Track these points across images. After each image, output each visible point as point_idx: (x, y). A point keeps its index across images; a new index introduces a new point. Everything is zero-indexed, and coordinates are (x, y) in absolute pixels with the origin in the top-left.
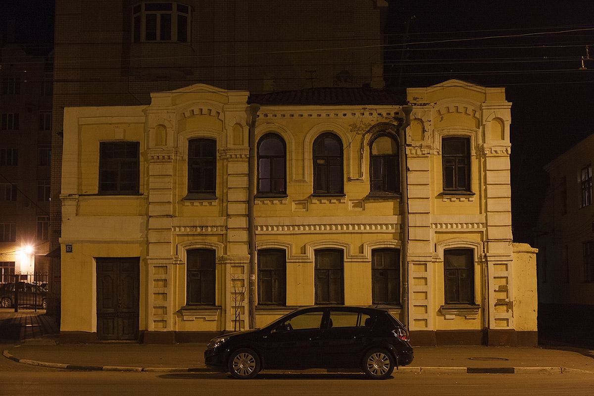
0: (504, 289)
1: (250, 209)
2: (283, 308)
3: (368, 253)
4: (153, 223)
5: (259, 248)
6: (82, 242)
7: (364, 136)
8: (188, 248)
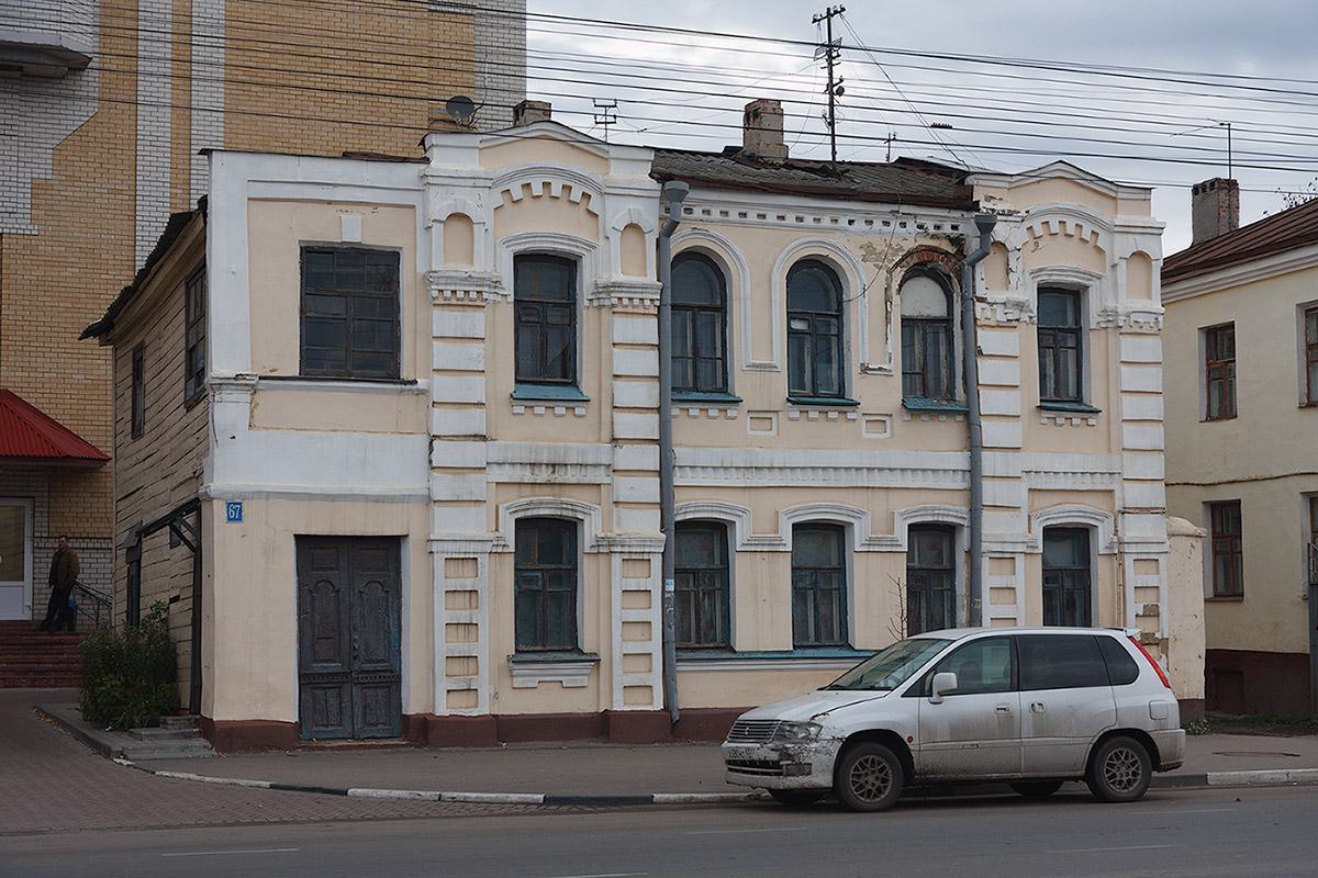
0: (1152, 612)
1: (664, 426)
2: (728, 655)
3: (902, 535)
4: (445, 453)
5: (678, 518)
6: (269, 495)
7: (890, 272)
8: (520, 515)
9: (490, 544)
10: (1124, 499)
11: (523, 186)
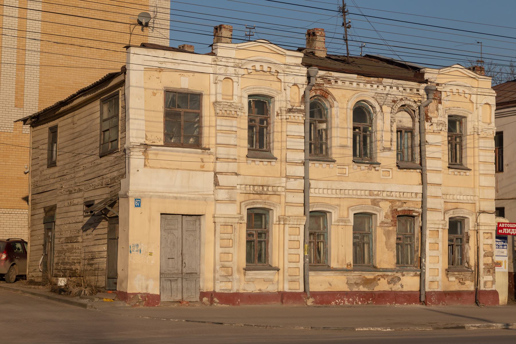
1: (306, 171)
9: (237, 219)
10: (480, 207)
11: (260, 66)
